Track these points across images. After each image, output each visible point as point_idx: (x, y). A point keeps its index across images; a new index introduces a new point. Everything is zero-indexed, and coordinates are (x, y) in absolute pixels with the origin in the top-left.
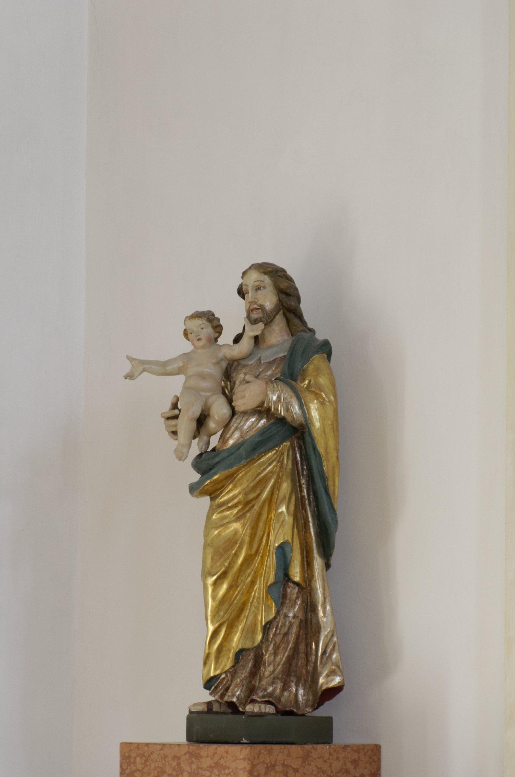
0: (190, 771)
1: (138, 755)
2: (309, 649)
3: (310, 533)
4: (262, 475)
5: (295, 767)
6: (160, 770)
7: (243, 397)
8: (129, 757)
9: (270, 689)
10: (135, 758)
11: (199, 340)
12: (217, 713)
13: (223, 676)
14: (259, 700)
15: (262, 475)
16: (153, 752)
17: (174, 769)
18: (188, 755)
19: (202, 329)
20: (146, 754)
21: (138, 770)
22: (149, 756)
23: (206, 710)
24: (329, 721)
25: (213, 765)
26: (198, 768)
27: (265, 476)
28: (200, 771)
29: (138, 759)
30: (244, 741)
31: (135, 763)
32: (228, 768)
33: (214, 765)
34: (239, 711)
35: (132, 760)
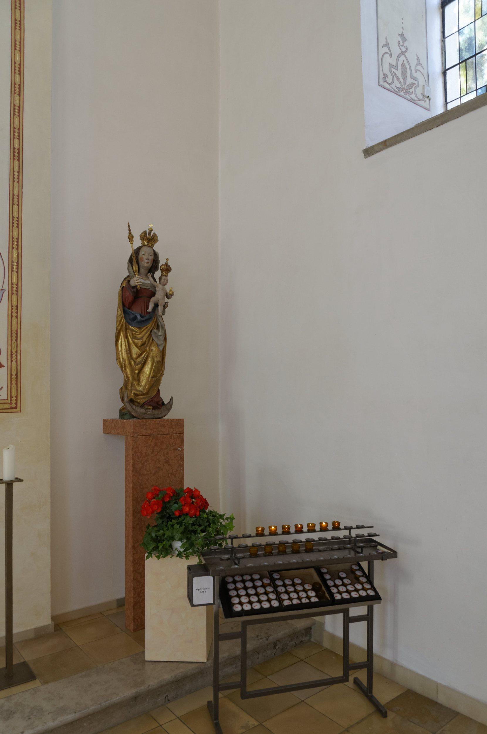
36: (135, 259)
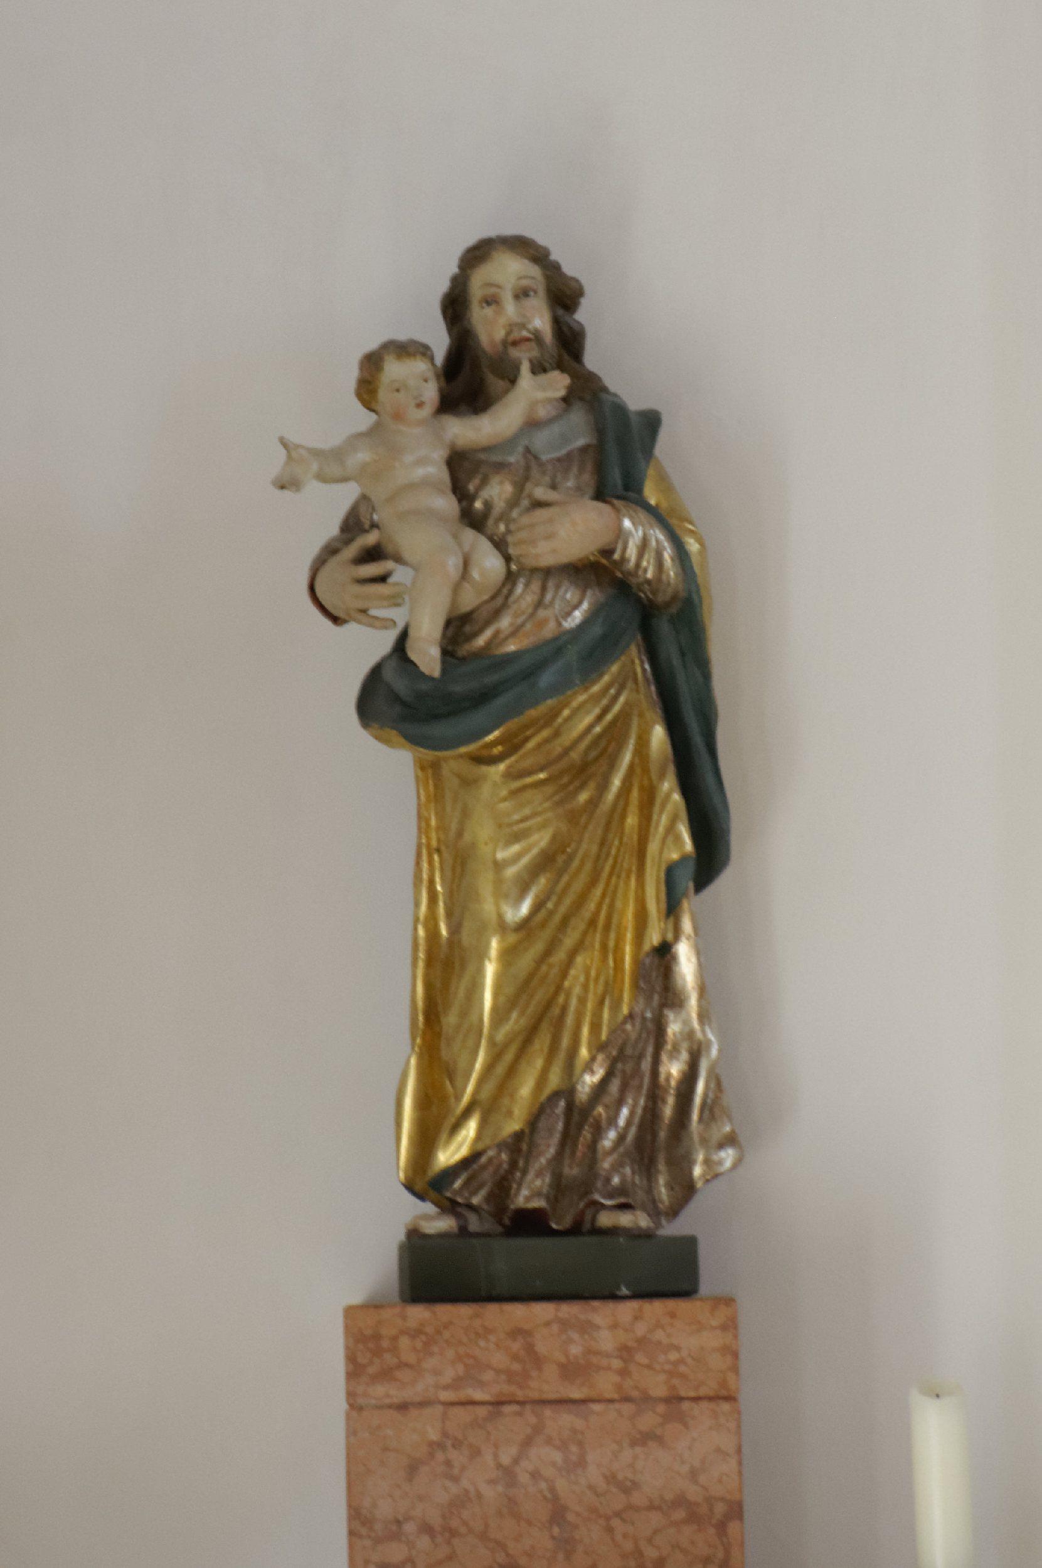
0: (563, 1360)
1: (402, 1332)
2: (711, 1095)
3: (445, 904)
4: (617, 708)
5: (541, 1348)
6: (471, 1361)
7: (550, 537)
8: (377, 1337)
9: (616, 1180)
10: (395, 1339)
11: (420, 405)
12: (477, 1235)
13: (491, 1153)
14: (608, 1202)
15: (617, 708)
16: (451, 1323)
17: (515, 1357)
18: (555, 1328)
19: (398, 390)
20: (429, 1330)
21: (407, 1365)
22: (438, 1332)
23: (456, 1230)
24: (687, 1248)
25: (630, 1344)
26: (589, 1351)
27: (621, 711)
28: (594, 1360)
29: (404, 1342)
30: (624, 1291)
31: (394, 1350)
32: (678, 1348)
33: (635, 1345)
34: (550, 1227)
35: (385, 1344)
36: (739, 1413)
